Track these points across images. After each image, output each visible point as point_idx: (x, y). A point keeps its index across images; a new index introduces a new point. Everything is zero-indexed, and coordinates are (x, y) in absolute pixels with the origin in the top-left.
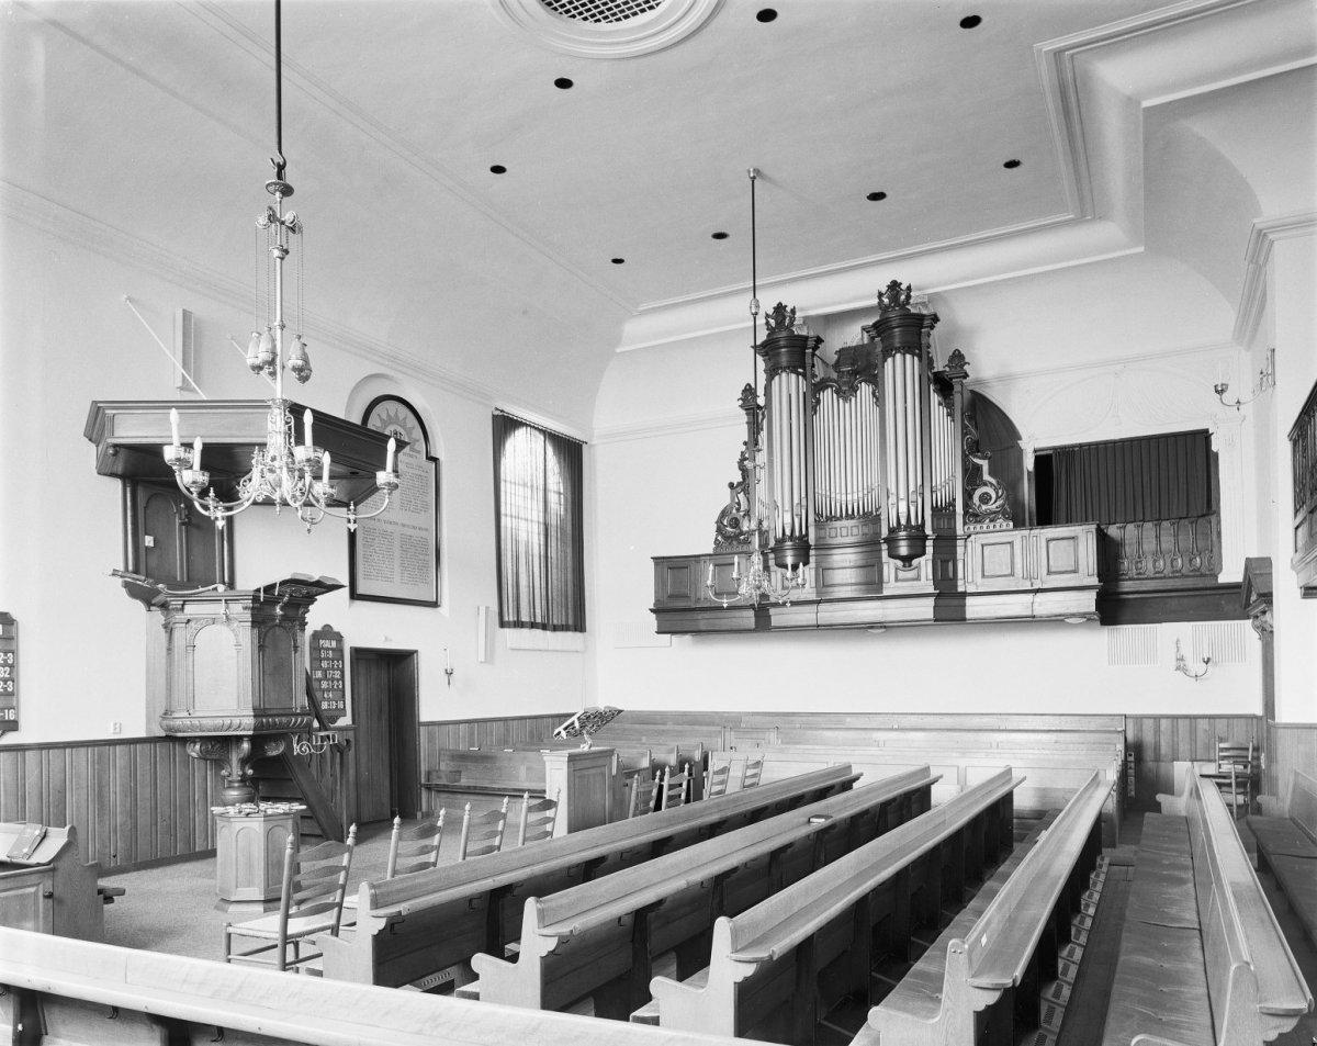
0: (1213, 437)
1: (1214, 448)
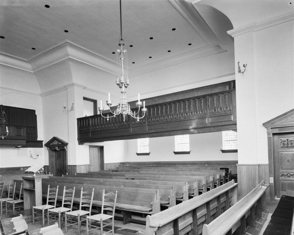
0: (36, 112)
1: (36, 114)
